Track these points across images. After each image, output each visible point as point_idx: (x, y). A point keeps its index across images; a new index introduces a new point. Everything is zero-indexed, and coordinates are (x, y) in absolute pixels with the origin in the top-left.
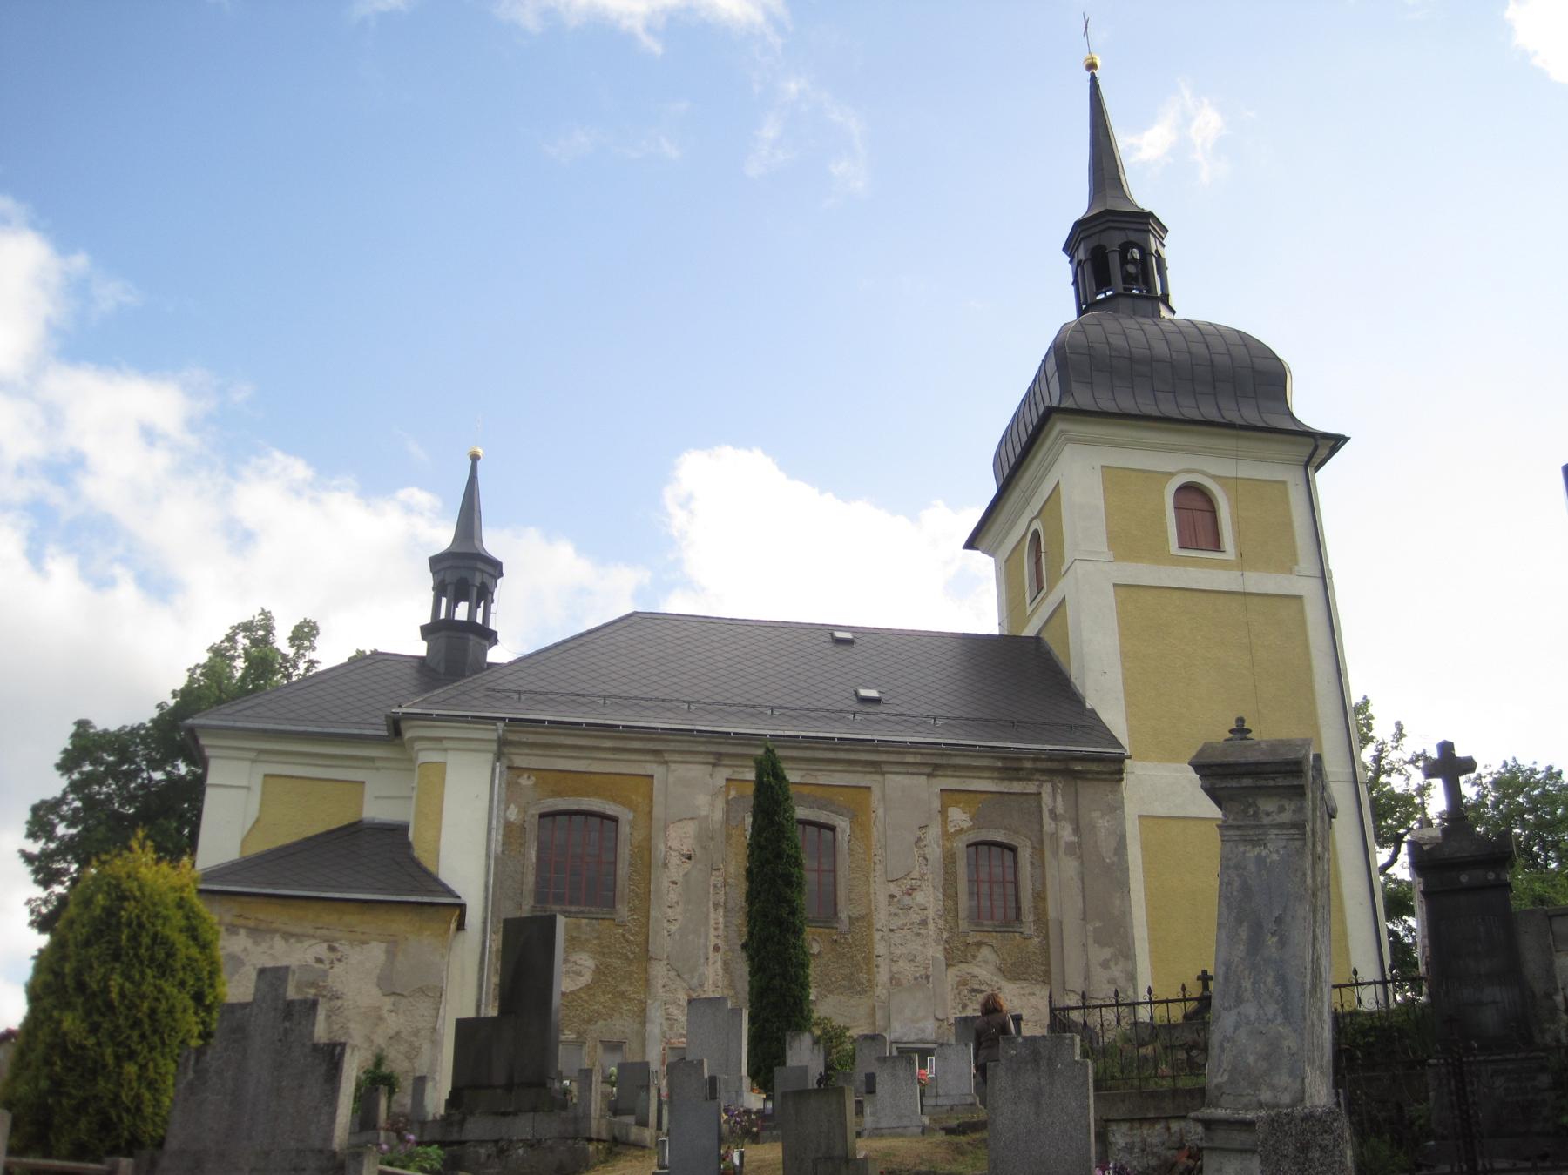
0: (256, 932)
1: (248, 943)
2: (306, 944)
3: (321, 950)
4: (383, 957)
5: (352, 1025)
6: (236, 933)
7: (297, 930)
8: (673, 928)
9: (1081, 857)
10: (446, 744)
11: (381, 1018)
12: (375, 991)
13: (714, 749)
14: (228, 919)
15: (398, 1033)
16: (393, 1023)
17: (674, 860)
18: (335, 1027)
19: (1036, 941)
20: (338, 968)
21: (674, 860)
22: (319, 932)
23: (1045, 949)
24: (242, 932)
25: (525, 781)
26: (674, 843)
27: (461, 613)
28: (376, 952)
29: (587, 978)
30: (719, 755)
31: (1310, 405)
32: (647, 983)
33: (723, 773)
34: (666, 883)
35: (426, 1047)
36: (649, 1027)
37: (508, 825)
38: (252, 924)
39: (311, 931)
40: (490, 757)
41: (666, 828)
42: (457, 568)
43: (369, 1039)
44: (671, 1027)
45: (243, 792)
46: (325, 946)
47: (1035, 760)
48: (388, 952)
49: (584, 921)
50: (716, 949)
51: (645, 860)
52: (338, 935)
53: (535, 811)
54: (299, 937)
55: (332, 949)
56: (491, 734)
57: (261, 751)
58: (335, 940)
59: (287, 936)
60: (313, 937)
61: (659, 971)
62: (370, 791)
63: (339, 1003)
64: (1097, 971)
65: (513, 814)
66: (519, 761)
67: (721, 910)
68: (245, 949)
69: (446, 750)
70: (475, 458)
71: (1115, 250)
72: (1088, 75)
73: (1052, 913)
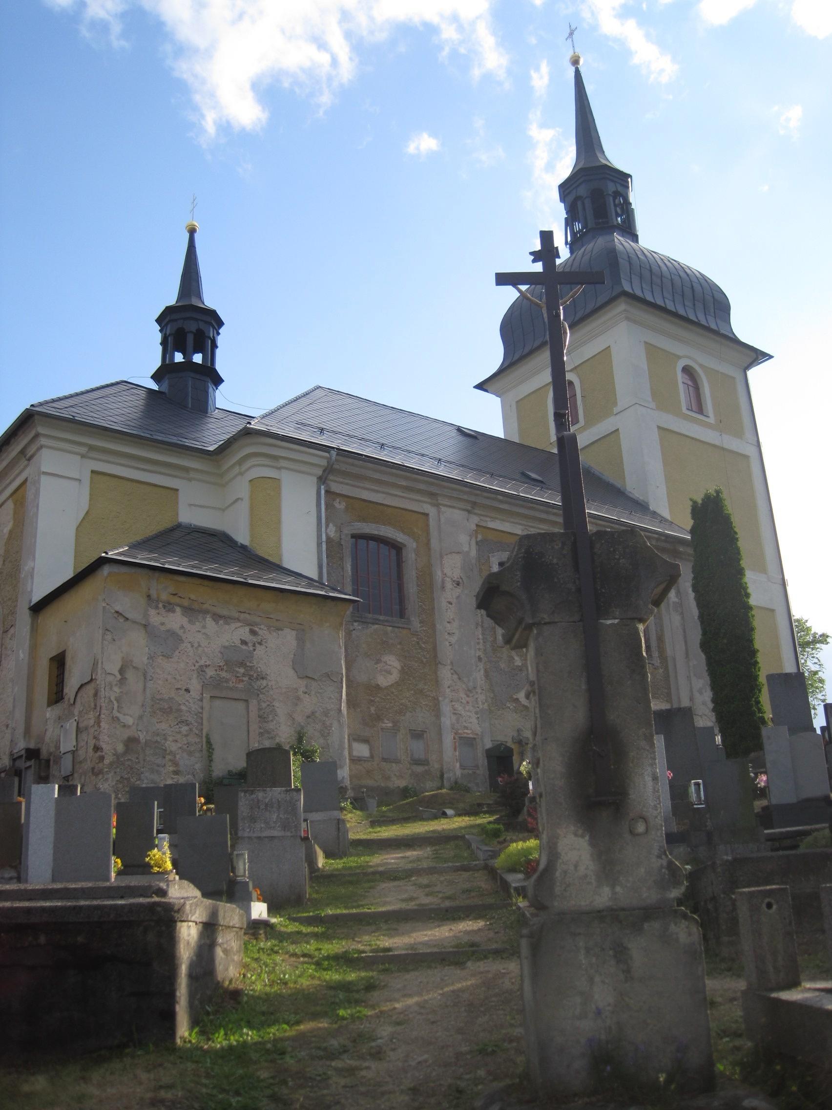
0: (190, 611)
1: (184, 621)
2: (233, 626)
3: (243, 632)
4: (294, 643)
5: (276, 704)
6: (174, 611)
7: (225, 612)
8: (453, 639)
9: (682, 614)
10: (283, 463)
11: (298, 698)
12: (291, 673)
13: (473, 499)
14: (164, 596)
15: (313, 713)
16: (309, 704)
17: (449, 585)
18: (264, 705)
19: (661, 671)
20: (260, 651)
21: (449, 585)
22: (243, 616)
23: (667, 677)
24: (178, 609)
25: (340, 505)
26: (447, 571)
27: (179, 357)
28: (289, 637)
29: (395, 677)
30: (474, 504)
31: (744, 325)
32: (437, 682)
33: (475, 520)
34: (444, 604)
35: (335, 725)
36: (443, 719)
37: (329, 540)
38: (186, 603)
39: (236, 615)
40: (315, 479)
41: (441, 557)
42: (176, 320)
43: (290, 716)
44: (458, 720)
45: (77, 483)
46: (247, 629)
47: (658, 540)
48: (297, 639)
49: (390, 629)
50: (480, 659)
51: (427, 583)
52: (258, 620)
53: (347, 531)
54: (227, 619)
55: (253, 632)
56: (320, 460)
57: (91, 448)
58: (257, 624)
59: (217, 617)
60: (238, 620)
61: (446, 674)
62: (184, 499)
63: (264, 683)
64: (697, 695)
65: (332, 531)
66: (335, 487)
67: (480, 629)
68: (182, 627)
69: (279, 468)
70: (192, 231)
71: (597, 194)
72: (573, 69)
73: (669, 652)
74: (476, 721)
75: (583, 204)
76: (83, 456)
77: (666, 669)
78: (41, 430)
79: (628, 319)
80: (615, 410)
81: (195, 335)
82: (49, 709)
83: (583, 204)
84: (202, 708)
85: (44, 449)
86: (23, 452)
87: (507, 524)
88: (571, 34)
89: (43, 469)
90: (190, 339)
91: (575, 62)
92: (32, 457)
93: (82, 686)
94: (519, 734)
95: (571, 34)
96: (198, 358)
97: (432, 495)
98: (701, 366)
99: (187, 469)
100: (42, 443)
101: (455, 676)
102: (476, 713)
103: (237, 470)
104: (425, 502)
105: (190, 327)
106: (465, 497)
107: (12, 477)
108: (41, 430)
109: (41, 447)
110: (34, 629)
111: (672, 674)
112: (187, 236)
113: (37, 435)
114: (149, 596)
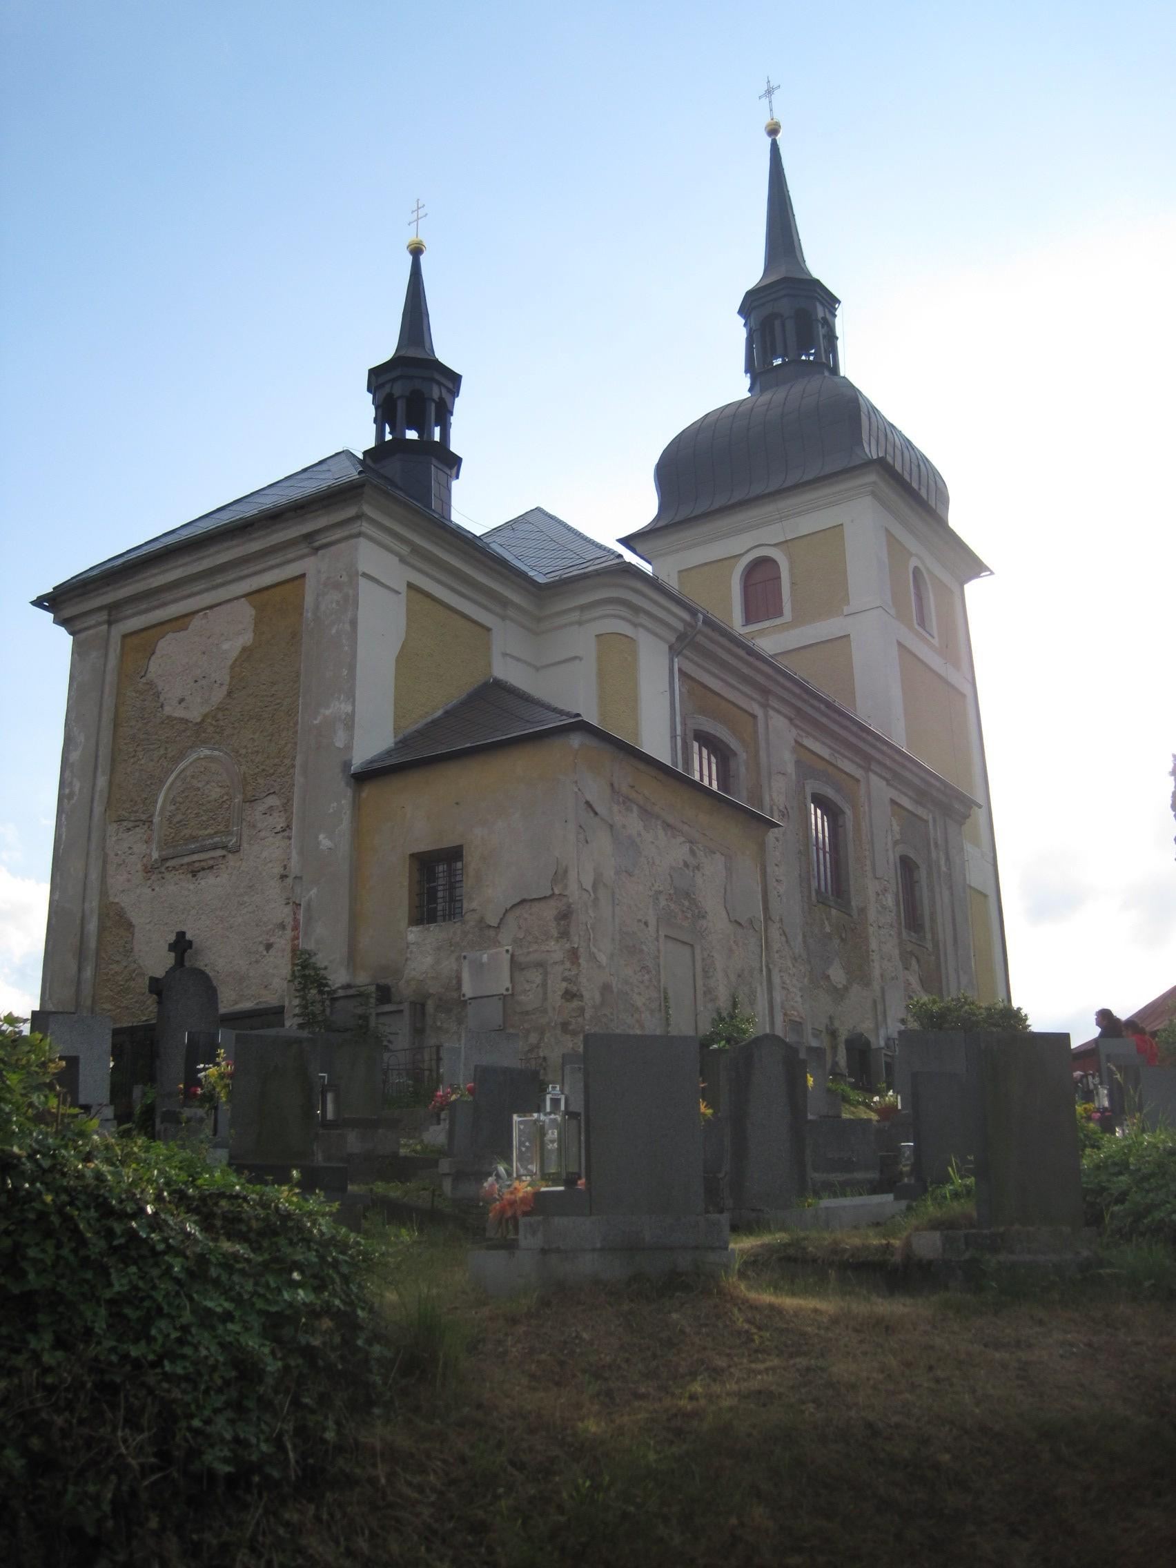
0: (647, 814)
10: (643, 619)
24: (635, 808)
40: (666, 647)
57: (416, 550)
59: (668, 826)
70: (416, 251)
71: (790, 316)
72: (769, 140)
74: (799, 1000)
75: (783, 325)
76: (402, 560)
77: (938, 958)
78: (367, 509)
79: (873, 494)
80: (846, 610)
81: (437, 403)
82: (414, 929)
83: (783, 325)
84: (658, 950)
85: (361, 539)
86: (308, 537)
87: (818, 744)
88: (769, 92)
89: (362, 567)
90: (401, 406)
91: (773, 131)
92: (317, 549)
93: (523, 901)
94: (832, 1023)
95: (769, 92)
96: (412, 435)
97: (765, 692)
98: (928, 569)
99: (505, 603)
100: (363, 529)
101: (783, 939)
102: (801, 990)
103: (575, 616)
104: (754, 699)
105: (414, 388)
106: (793, 701)
107: (246, 572)
108: (367, 509)
109: (359, 535)
110: (357, 806)
111: (943, 965)
112: (409, 259)
113: (359, 517)
114: (612, 785)
